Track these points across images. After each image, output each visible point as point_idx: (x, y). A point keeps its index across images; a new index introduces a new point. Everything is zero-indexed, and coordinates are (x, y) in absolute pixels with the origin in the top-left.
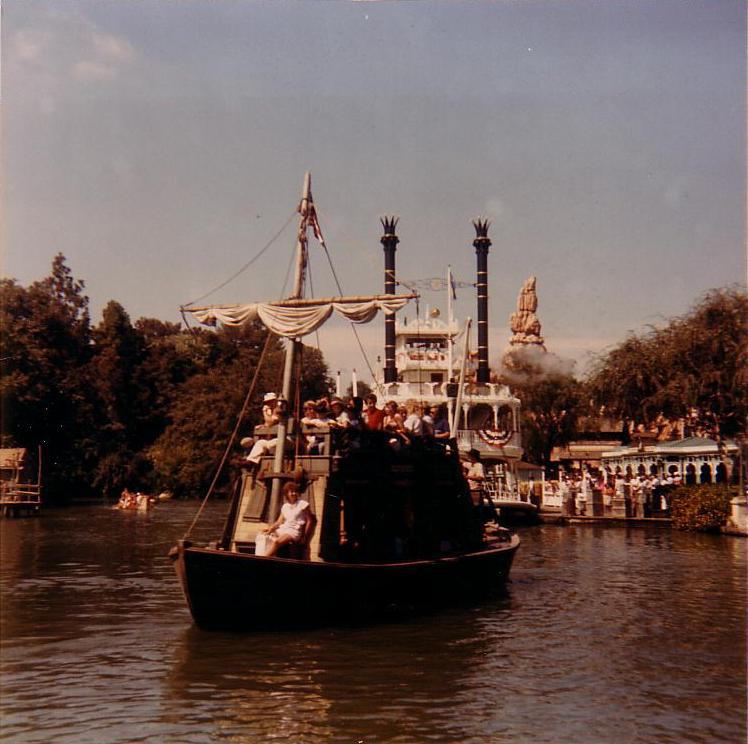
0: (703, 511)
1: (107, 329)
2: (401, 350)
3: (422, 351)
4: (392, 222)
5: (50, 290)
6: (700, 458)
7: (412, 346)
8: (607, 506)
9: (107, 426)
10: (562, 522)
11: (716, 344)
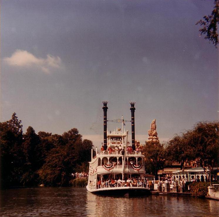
0: (200, 191)
1: (28, 135)
2: (109, 141)
3: (115, 141)
4: (106, 102)
5: (11, 123)
6: (201, 173)
7: (113, 140)
8: (171, 189)
9: (26, 164)
10: (157, 194)
11: (200, 139)
